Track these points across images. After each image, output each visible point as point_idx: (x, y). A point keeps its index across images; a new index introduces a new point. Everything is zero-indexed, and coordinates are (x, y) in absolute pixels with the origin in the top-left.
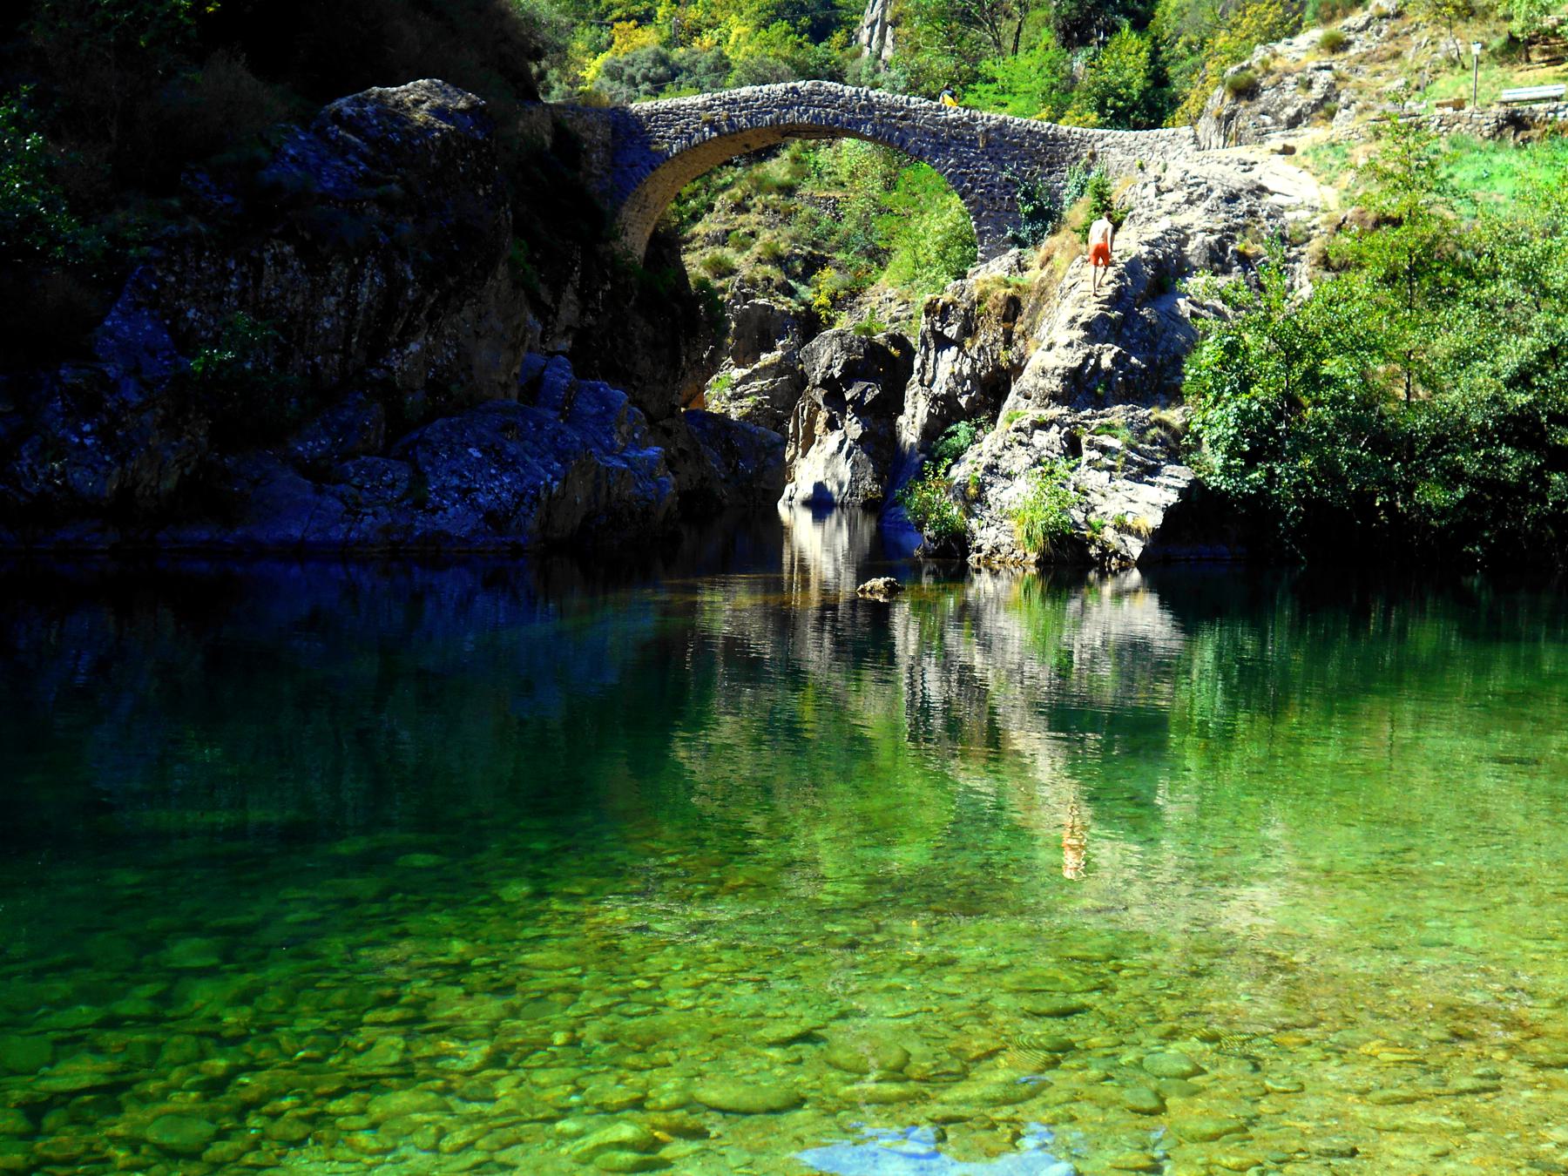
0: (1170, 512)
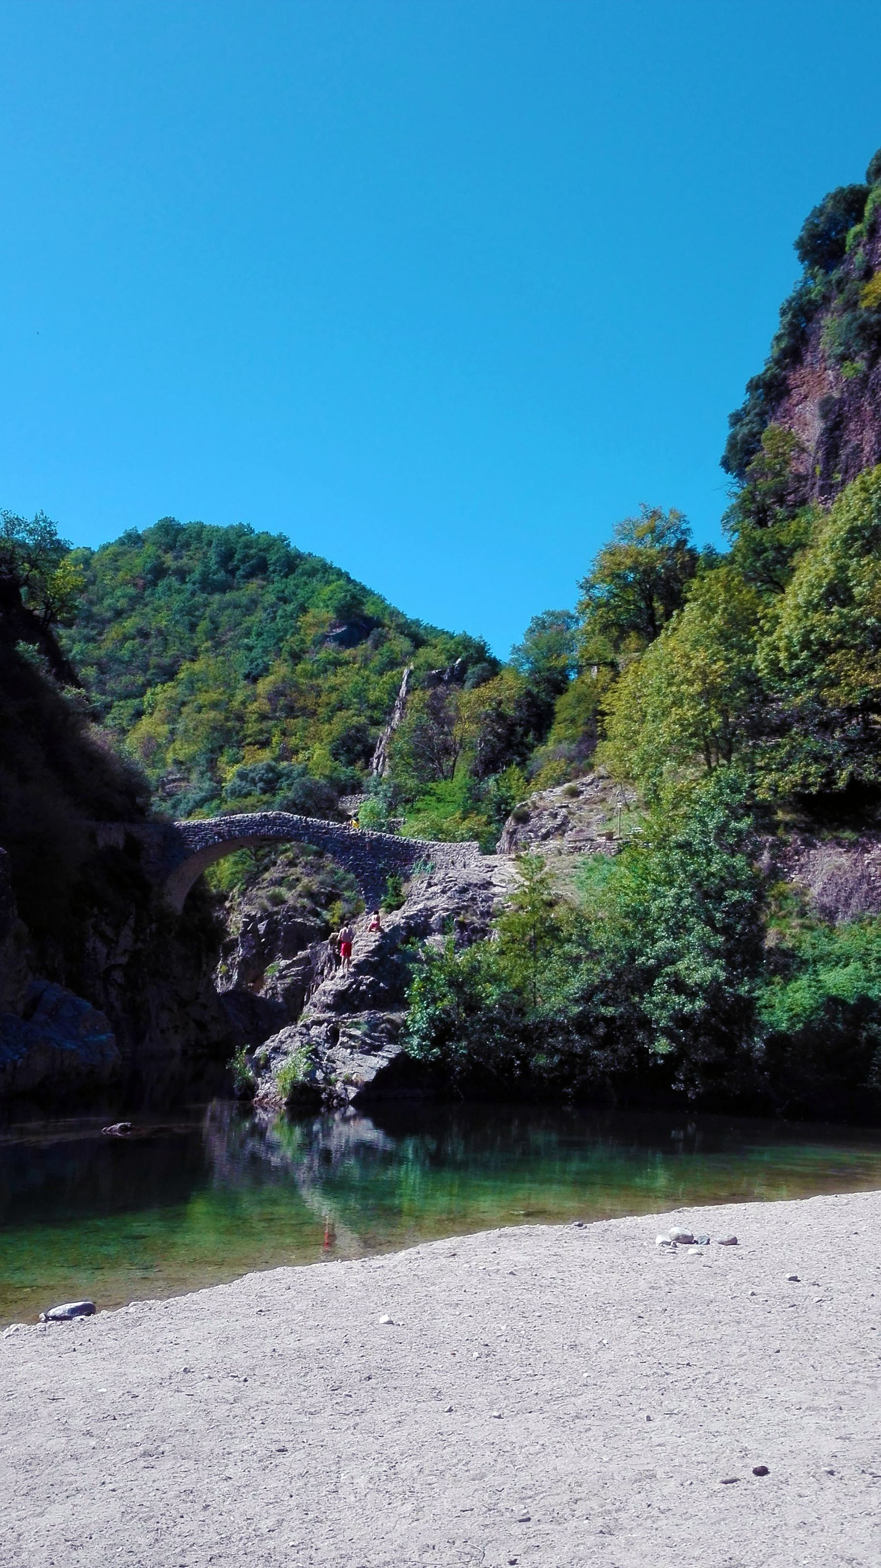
0: (381, 1072)
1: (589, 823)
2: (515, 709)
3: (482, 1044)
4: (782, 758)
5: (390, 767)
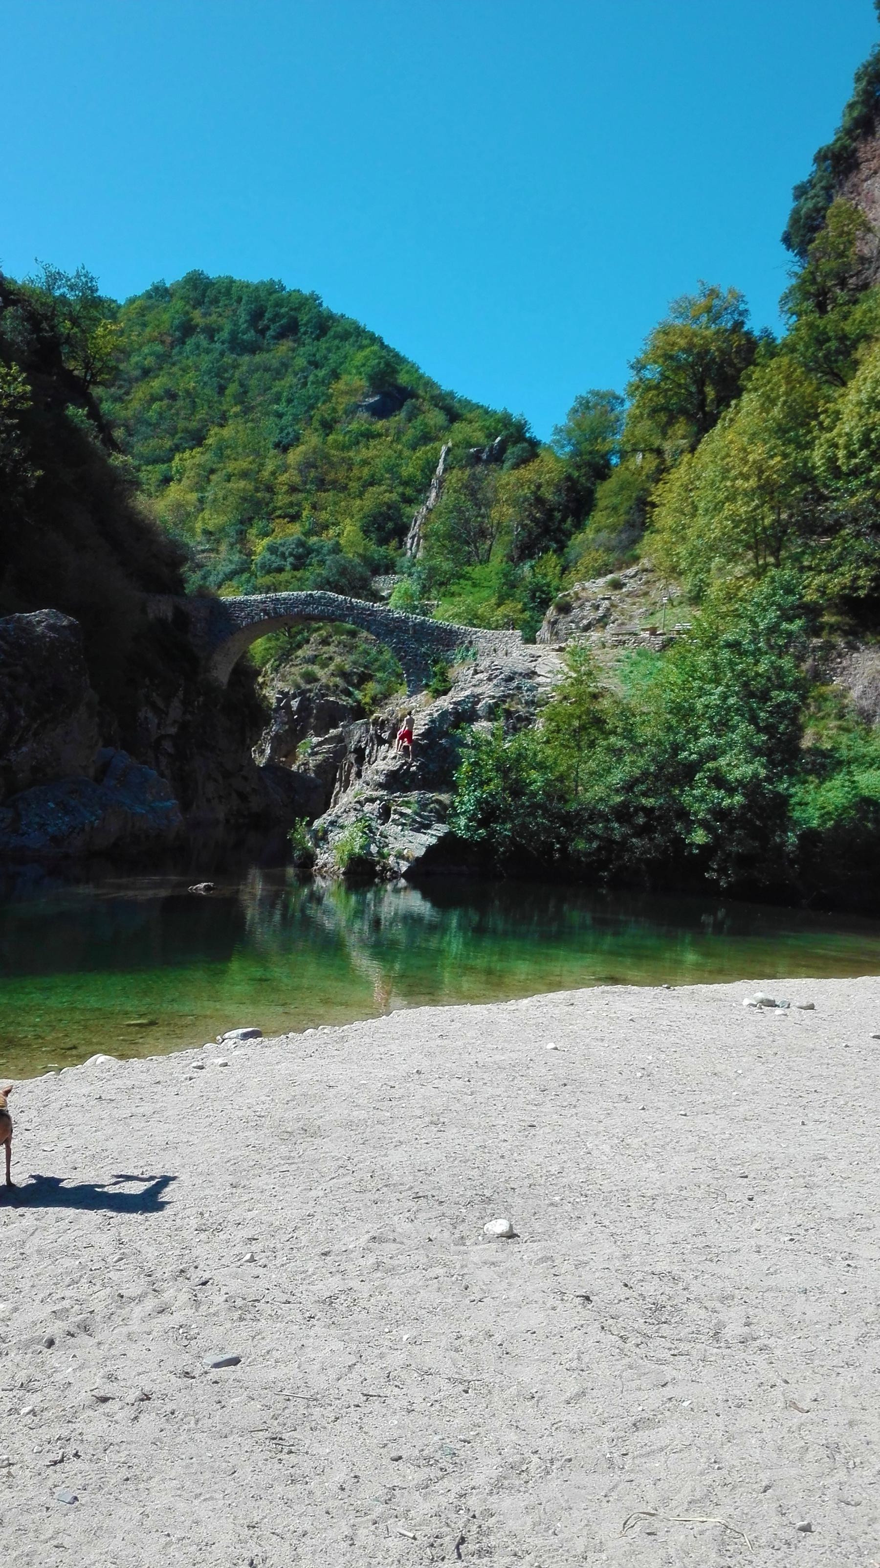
0: (430, 849)
1: (631, 617)
2: (554, 493)
3: (524, 826)
4: (832, 559)
5: (425, 548)
